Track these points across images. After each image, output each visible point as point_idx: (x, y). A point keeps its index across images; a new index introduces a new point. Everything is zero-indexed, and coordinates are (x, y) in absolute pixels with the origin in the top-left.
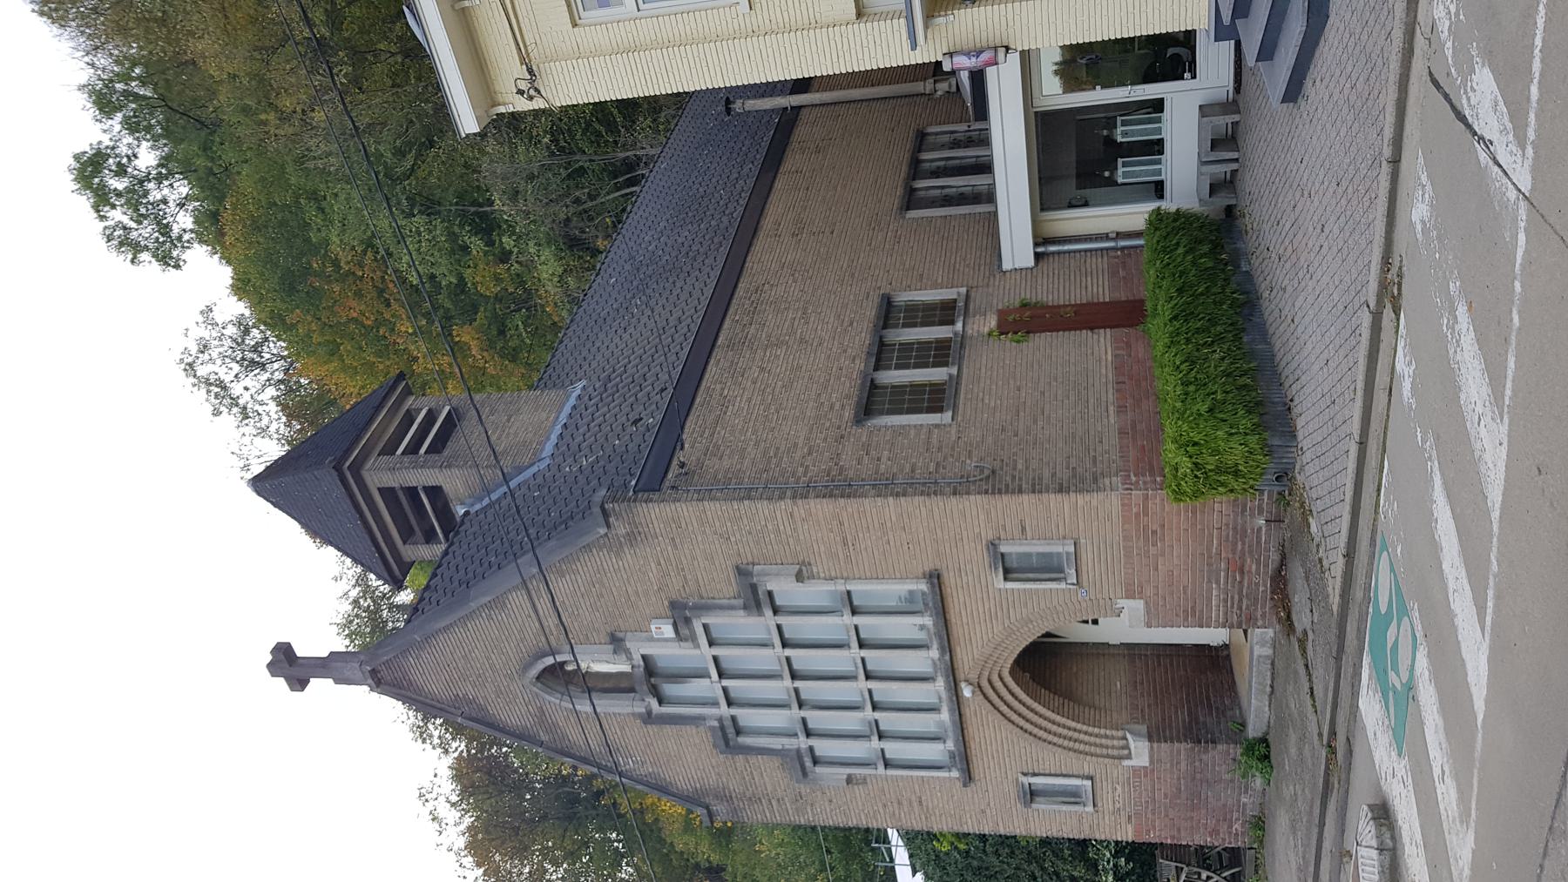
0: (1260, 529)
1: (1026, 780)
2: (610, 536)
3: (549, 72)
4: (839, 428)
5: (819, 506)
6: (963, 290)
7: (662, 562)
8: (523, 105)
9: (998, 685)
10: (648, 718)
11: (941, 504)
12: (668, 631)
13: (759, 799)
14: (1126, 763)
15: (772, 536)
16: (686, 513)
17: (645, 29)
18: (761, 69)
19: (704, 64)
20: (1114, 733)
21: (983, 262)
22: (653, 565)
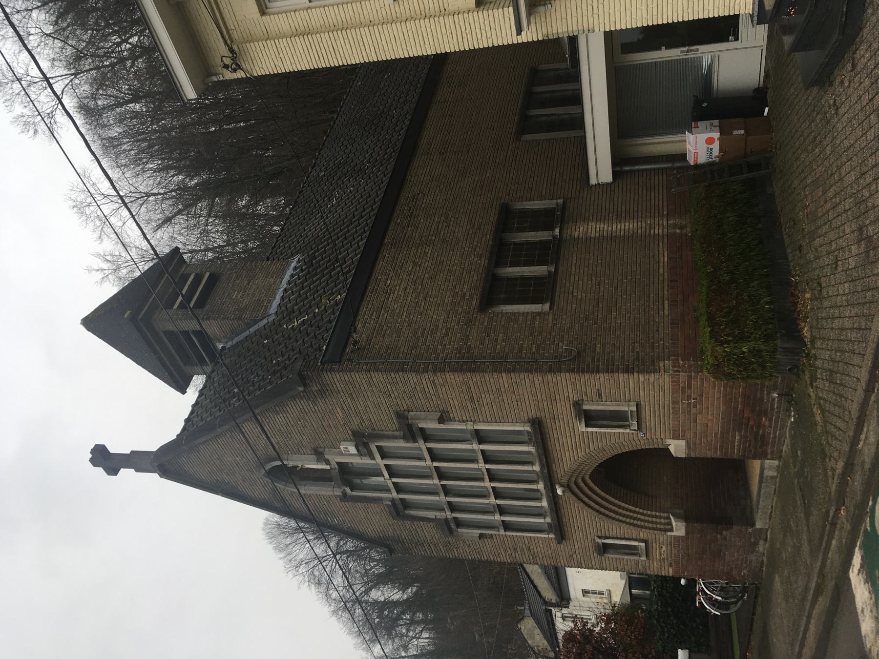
0: (773, 399)
1: (600, 541)
2: (307, 391)
3: (246, 50)
4: (468, 313)
5: (452, 377)
6: (560, 201)
7: (345, 408)
8: (229, 75)
9: (582, 485)
10: (345, 497)
11: (540, 378)
12: (353, 450)
13: (422, 544)
14: (669, 533)
15: (420, 394)
16: (358, 379)
17: (316, 16)
18: (404, 47)
19: (361, 44)
20: (662, 514)
21: (575, 178)
22: (338, 409)
